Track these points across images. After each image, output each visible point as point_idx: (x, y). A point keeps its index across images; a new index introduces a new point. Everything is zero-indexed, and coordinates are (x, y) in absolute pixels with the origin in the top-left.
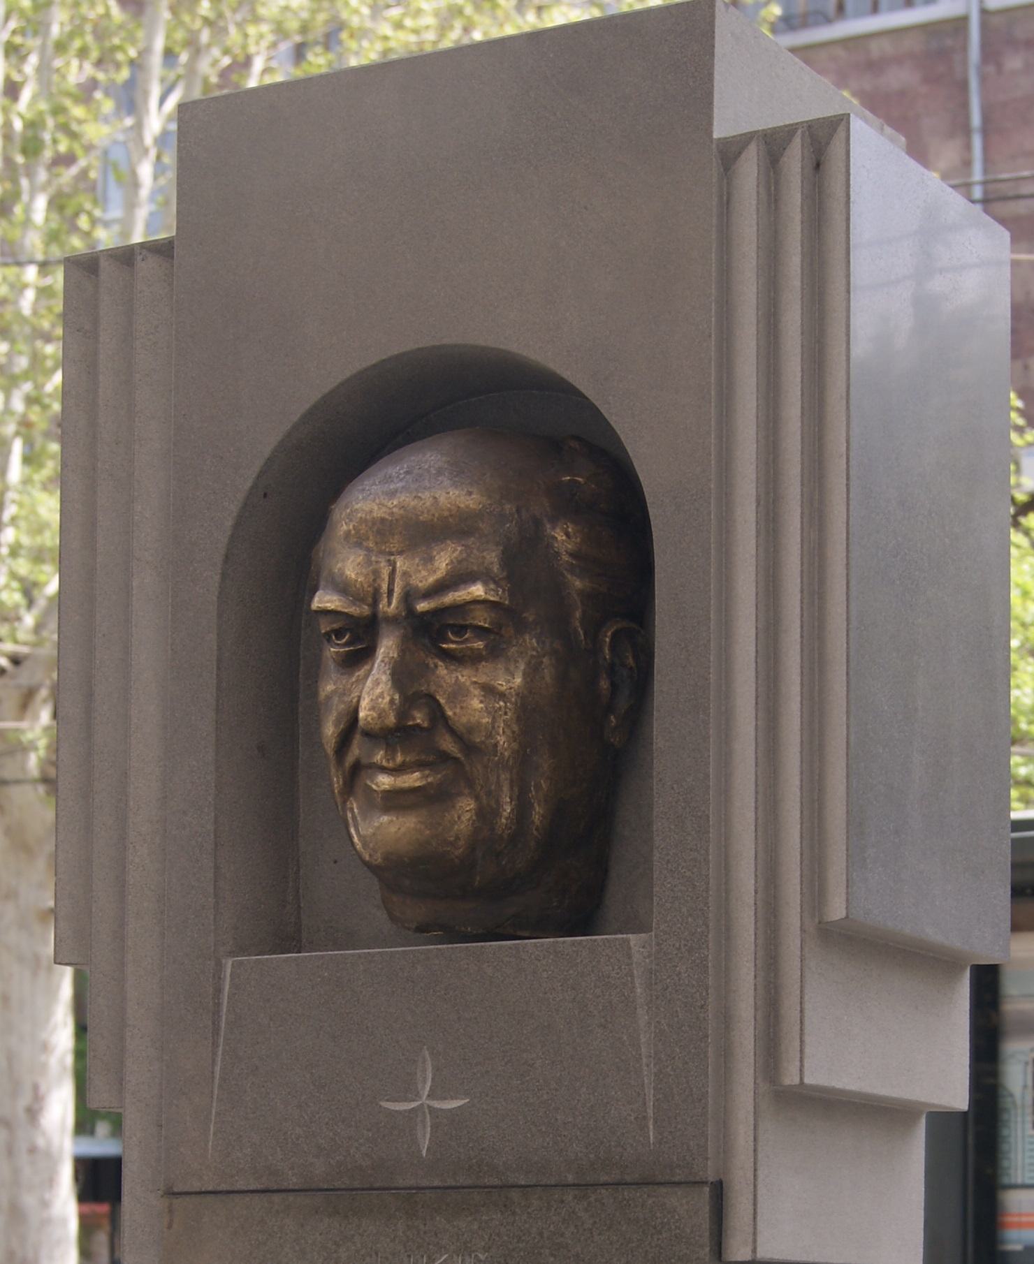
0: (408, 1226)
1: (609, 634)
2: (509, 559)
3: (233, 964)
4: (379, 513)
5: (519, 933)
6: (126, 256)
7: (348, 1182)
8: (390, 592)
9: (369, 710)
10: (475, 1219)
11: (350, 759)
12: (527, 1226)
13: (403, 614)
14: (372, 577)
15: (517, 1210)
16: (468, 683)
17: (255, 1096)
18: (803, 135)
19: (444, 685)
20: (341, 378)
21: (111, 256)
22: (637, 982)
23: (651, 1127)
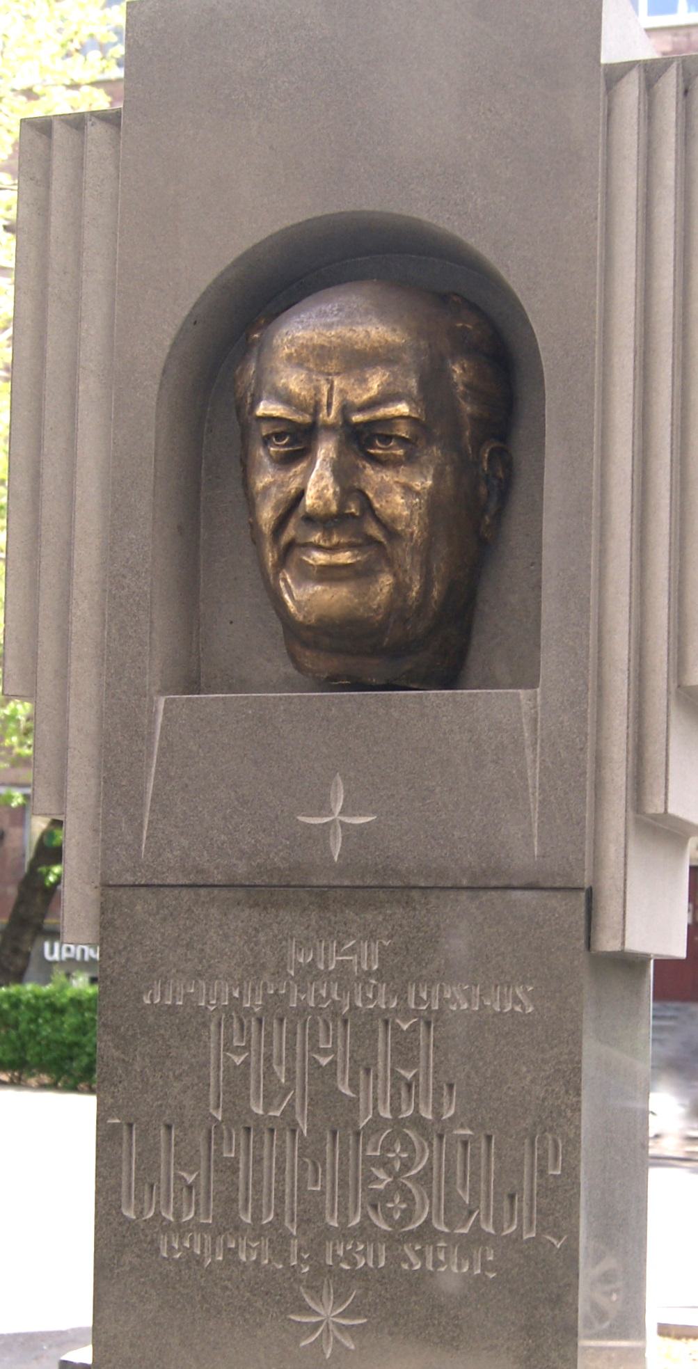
0: (320, 917)
1: (488, 450)
2: (422, 385)
3: (166, 701)
4: (318, 340)
5: (412, 686)
6: (77, 122)
7: (267, 880)
8: (329, 405)
9: (316, 498)
10: (380, 913)
11: (286, 538)
12: (426, 919)
13: (340, 423)
14: (313, 392)
15: (417, 906)
16: (391, 482)
17: (185, 808)
18: (678, 68)
19: (372, 482)
20: (270, 232)
21: (62, 120)
22: (525, 728)
23: (536, 843)
